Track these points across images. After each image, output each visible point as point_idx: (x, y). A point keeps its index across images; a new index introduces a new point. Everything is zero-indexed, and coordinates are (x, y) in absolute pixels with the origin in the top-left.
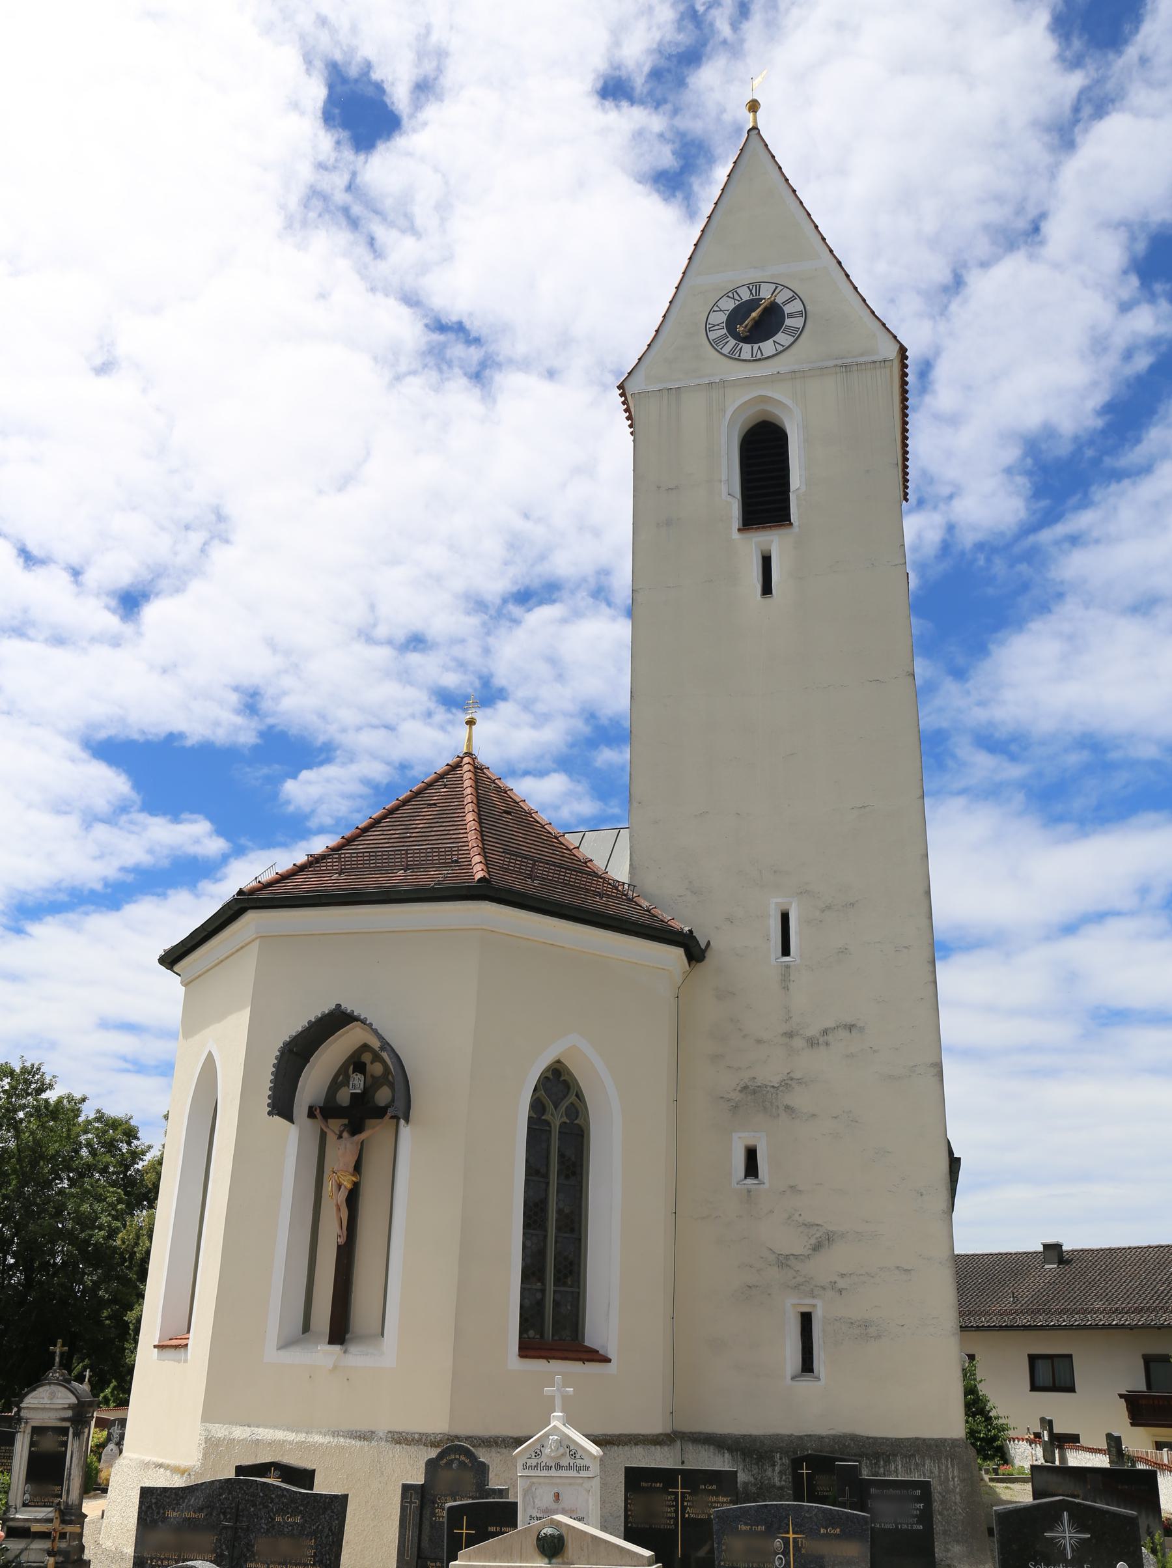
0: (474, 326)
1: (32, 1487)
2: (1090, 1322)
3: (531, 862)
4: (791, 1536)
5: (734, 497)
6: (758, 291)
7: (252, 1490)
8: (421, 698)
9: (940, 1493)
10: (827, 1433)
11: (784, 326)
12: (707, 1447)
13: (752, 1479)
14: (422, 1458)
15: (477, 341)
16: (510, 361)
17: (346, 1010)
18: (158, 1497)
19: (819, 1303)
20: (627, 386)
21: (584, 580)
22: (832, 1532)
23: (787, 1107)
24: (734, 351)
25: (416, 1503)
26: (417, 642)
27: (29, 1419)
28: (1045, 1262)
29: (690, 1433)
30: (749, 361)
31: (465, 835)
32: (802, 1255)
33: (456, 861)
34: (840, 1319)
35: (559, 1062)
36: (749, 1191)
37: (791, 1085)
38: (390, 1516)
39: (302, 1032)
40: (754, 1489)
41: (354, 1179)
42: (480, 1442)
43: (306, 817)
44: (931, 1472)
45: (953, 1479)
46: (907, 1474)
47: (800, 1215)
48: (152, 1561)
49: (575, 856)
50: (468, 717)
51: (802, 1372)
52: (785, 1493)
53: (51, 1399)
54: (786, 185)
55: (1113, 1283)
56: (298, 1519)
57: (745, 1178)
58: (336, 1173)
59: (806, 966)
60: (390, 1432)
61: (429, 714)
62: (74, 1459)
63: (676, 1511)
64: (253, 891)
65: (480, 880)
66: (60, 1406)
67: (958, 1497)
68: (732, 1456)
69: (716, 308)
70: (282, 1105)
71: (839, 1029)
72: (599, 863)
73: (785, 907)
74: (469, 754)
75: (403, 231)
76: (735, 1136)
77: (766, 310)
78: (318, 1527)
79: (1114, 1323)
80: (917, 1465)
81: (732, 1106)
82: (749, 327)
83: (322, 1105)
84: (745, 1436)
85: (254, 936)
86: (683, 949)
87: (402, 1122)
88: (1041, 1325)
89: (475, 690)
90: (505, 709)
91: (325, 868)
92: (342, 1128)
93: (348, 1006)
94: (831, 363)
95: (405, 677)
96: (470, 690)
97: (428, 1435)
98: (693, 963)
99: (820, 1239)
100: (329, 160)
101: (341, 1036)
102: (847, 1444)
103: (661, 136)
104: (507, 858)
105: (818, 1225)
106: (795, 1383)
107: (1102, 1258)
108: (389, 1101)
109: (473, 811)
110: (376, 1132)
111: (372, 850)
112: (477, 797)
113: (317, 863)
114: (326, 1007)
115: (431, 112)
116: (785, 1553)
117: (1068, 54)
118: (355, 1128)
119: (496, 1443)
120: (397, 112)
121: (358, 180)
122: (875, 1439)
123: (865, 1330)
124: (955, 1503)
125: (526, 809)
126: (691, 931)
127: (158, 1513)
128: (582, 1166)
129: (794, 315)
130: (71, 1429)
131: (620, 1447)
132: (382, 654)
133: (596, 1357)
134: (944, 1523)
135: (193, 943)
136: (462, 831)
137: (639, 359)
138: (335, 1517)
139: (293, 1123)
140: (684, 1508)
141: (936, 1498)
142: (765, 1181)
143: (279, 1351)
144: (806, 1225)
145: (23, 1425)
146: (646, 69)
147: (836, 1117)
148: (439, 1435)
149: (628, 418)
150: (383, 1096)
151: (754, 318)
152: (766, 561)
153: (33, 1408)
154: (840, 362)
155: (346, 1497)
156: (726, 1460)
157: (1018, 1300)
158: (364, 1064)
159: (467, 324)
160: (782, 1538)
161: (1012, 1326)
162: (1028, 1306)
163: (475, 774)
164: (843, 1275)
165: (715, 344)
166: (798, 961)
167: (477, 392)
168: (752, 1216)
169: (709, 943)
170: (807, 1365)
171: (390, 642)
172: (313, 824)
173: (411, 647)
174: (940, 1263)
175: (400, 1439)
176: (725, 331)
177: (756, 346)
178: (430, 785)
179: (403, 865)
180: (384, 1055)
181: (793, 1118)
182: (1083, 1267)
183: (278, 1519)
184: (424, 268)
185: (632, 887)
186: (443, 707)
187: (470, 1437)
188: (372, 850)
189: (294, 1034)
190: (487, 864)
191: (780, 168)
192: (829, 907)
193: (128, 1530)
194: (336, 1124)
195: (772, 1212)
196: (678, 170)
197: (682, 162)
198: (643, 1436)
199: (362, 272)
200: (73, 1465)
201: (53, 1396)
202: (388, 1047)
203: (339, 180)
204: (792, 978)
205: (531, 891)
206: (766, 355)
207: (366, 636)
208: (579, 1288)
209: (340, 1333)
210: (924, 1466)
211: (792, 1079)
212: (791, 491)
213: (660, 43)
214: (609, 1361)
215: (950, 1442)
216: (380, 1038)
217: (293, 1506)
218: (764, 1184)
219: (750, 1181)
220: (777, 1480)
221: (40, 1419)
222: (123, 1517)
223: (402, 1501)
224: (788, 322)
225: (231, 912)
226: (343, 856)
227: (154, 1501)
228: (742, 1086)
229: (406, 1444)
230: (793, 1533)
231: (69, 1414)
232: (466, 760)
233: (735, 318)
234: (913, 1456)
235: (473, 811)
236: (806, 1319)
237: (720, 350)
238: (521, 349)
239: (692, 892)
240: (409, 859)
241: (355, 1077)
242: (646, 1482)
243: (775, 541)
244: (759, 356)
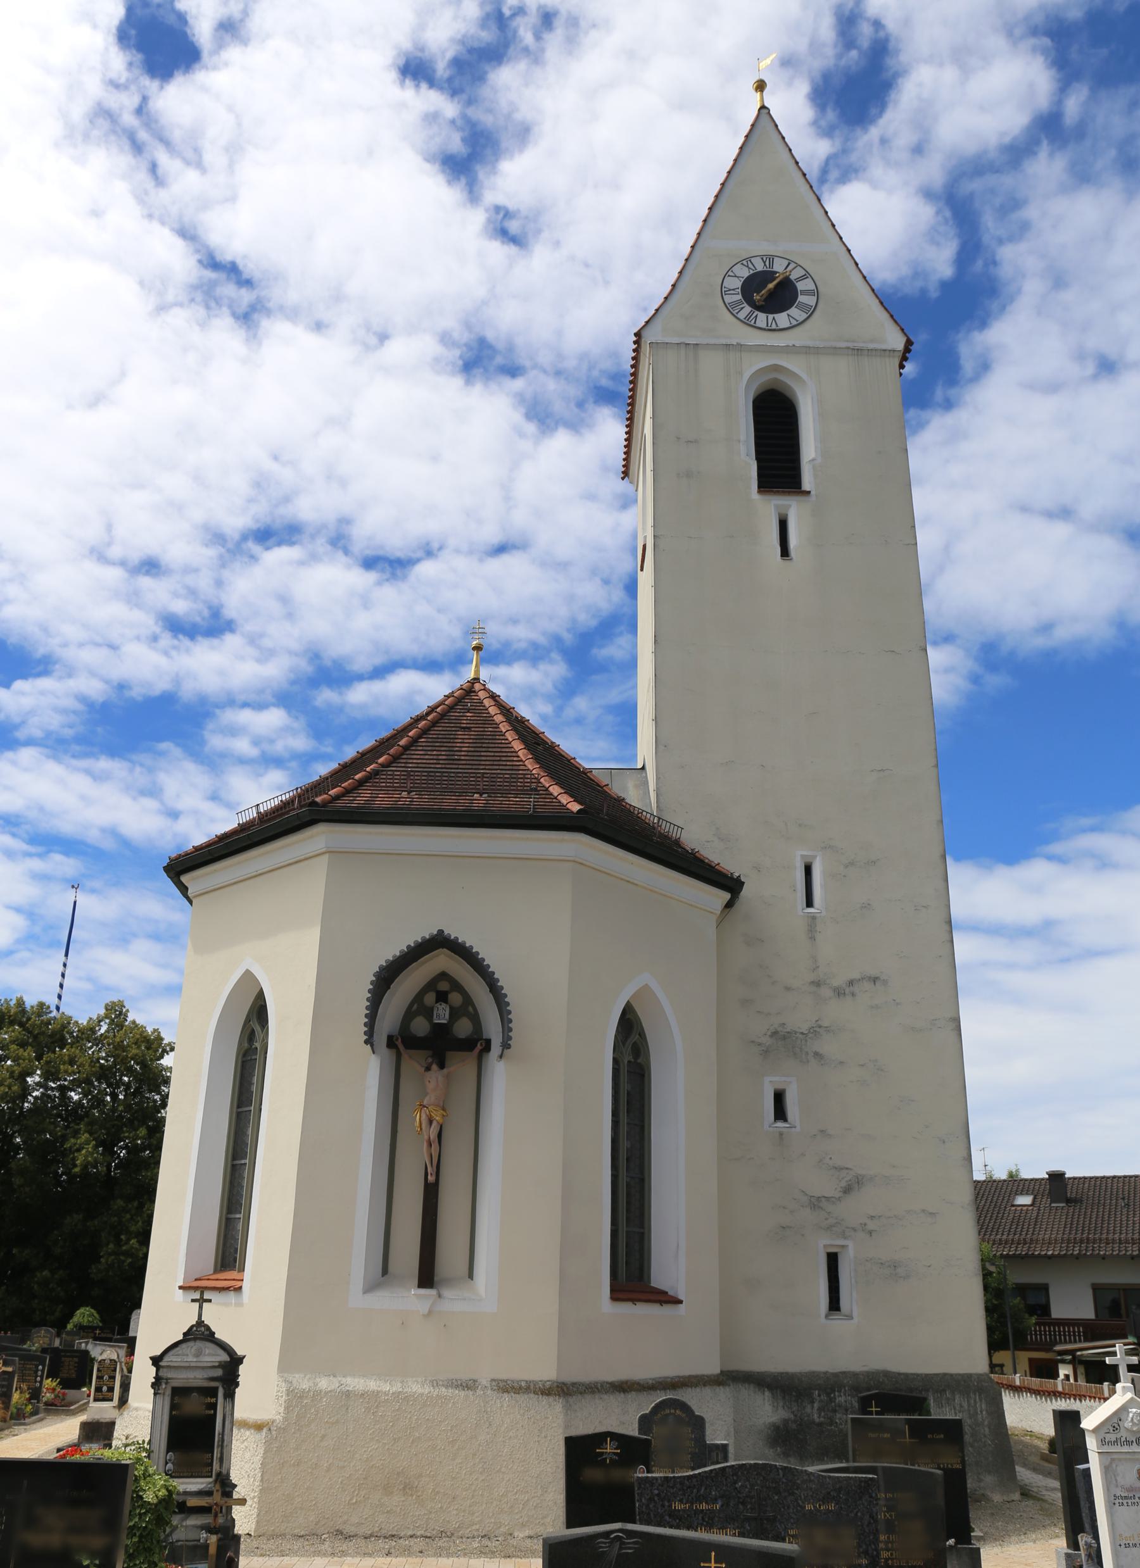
0: (249, 268)
1: (175, 1456)
8: (148, 622)
9: (970, 1426)
10: (861, 1370)
11: (797, 302)
12: (747, 1385)
13: (792, 1416)
14: (534, 1407)
15: (248, 283)
16: (281, 308)
17: (450, 936)
19: (850, 1244)
20: (644, 334)
21: (324, 526)
23: (816, 1054)
24: (750, 317)
26: (151, 566)
27: (170, 1379)
29: (728, 1371)
30: (764, 329)
32: (832, 1197)
33: (535, 790)
34: (871, 1259)
36: (781, 1134)
37: (819, 1032)
38: (501, 1468)
39: (400, 957)
40: (794, 1426)
43: (16, 727)
44: (961, 1406)
45: (981, 1412)
46: (939, 1408)
47: (831, 1158)
52: (824, 1429)
54: (796, 168)
58: (427, 1108)
59: (832, 918)
61: (155, 638)
62: (227, 1423)
67: (987, 1429)
68: (772, 1394)
71: (864, 981)
75: (187, 163)
76: (767, 1080)
78: (856, 1514)
80: (948, 1399)
81: (763, 1050)
82: (764, 297)
84: (782, 1373)
85: (324, 850)
89: (203, 619)
90: (232, 641)
94: (843, 345)
95: (134, 599)
96: (198, 619)
97: (535, 1383)
99: (850, 1183)
100: (120, 78)
101: (426, 962)
102: (881, 1380)
103: (453, 122)
105: (847, 1169)
106: (829, 1322)
111: (466, 771)
115: (233, 53)
117: (823, 123)
120: (197, 44)
121: (151, 104)
122: (906, 1375)
123: (894, 1270)
124: (985, 1436)
127: (663, 1506)
129: (806, 293)
131: (693, 1388)
132: (114, 575)
134: (975, 1454)
137: (656, 310)
141: (967, 1431)
144: (836, 1168)
145: (164, 1386)
146: (450, 55)
147: (862, 1065)
148: (548, 1383)
150: (463, 1028)
151: (770, 290)
152: (783, 525)
153: (174, 1367)
154: (851, 345)
156: (766, 1398)
159: (240, 264)
164: (872, 1217)
166: (824, 913)
167: (242, 333)
168: (784, 1158)
170: (834, 1304)
171: (123, 563)
172: (20, 735)
173: (144, 570)
174: (962, 1207)
176: (740, 297)
177: (771, 316)
178: (451, 708)
181: (822, 1065)
184: (205, 204)
186: (170, 633)
188: (466, 771)
191: (790, 150)
192: (852, 864)
195: (803, 1155)
196: (465, 156)
197: (469, 150)
198: (707, 1376)
199: (141, 198)
201: (198, 1354)
203: (126, 102)
204: (818, 929)
206: (781, 326)
207: (99, 555)
210: (954, 1400)
213: (464, 36)
214: (681, 1302)
215: (976, 1377)
219: (780, 1124)
220: (816, 1416)
221: (183, 1379)
226: (412, 773)
228: (773, 1031)
229: (515, 1393)
231: (219, 1373)
233: (751, 286)
234: (944, 1390)
236: (833, 1260)
237: (736, 315)
238: (292, 297)
239: (719, 838)
241: (439, 1006)
243: (796, 510)
244: (774, 326)
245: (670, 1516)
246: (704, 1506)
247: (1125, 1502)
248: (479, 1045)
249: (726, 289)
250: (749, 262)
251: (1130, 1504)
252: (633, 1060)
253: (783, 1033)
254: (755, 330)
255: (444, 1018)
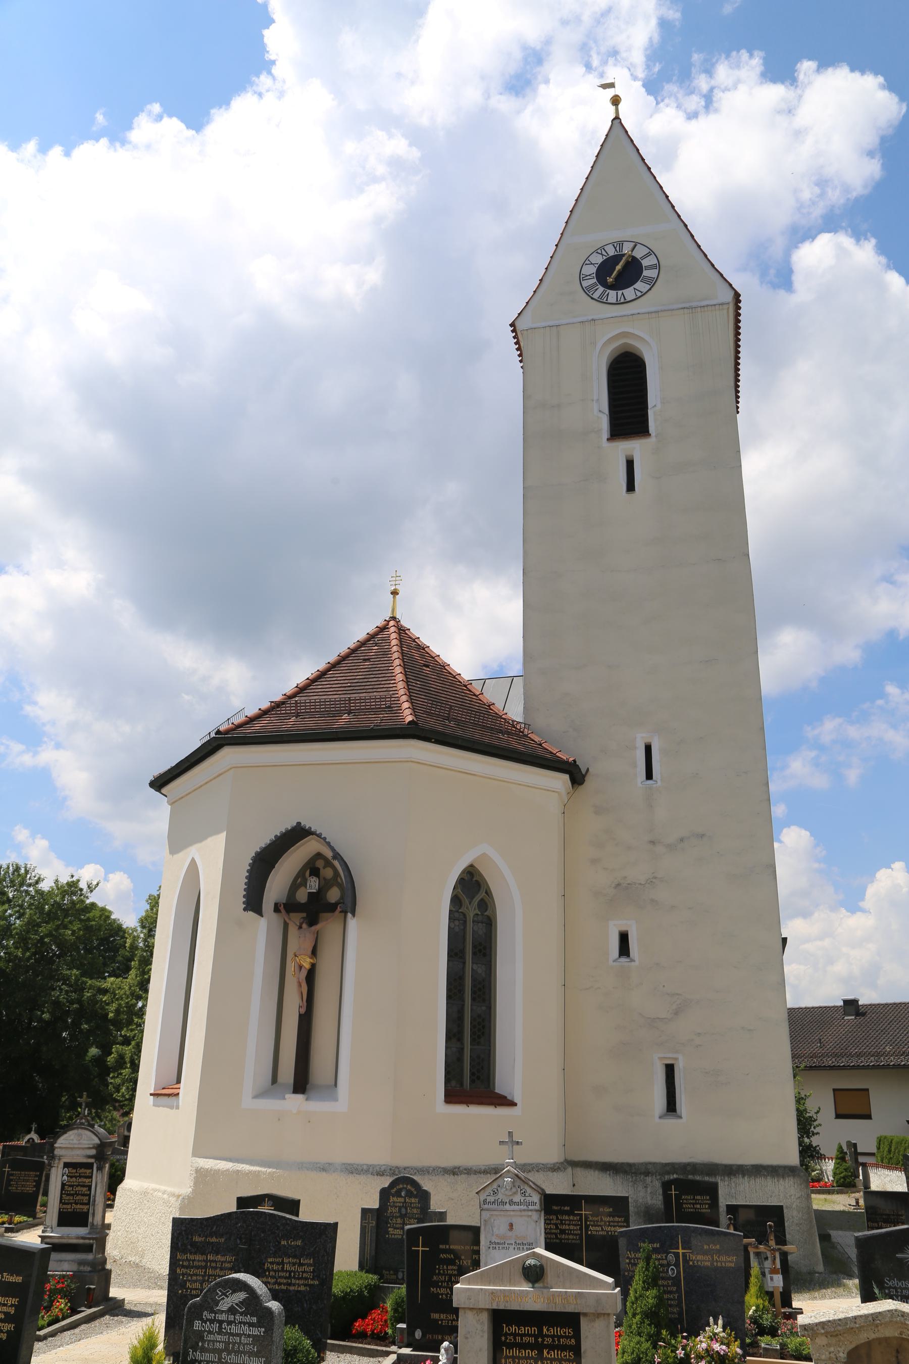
2: (883, 1063)
3: (448, 707)
4: (681, 1251)
5: (602, 412)
6: (621, 249)
7: (262, 1219)
17: (305, 827)
18: (187, 1226)
19: (680, 1057)
20: (517, 324)
22: (714, 1248)
23: (652, 900)
25: (372, 1223)
27: (62, 1156)
28: (846, 1014)
30: (650, 289)
31: (394, 685)
33: (389, 707)
35: (471, 866)
39: (270, 845)
41: (312, 961)
42: (415, 1171)
48: (183, 1277)
49: (480, 700)
50: (393, 589)
51: (667, 1111)
53: (79, 1140)
55: (900, 1031)
56: (299, 1243)
57: (619, 957)
60: (344, 1164)
62: (98, 1188)
63: (581, 1229)
64: (227, 732)
65: (410, 723)
66: (87, 1146)
68: (613, 1180)
69: (587, 262)
70: (254, 903)
72: (499, 706)
73: (648, 741)
74: (393, 618)
76: (611, 924)
77: (627, 264)
78: (315, 1249)
79: (903, 1063)
83: (284, 902)
86: (568, 775)
87: (349, 915)
88: (844, 1066)
91: (284, 712)
92: (302, 920)
93: (307, 823)
97: (374, 1166)
98: (576, 785)
104: (430, 703)
106: (662, 1121)
107: (891, 1010)
108: (338, 899)
109: (400, 665)
110: (329, 926)
112: (402, 653)
113: (278, 707)
114: (289, 824)
116: (677, 1265)
118: (312, 921)
119: (428, 1172)
125: (441, 662)
126: (574, 761)
127: (187, 1238)
128: (491, 948)
130: (95, 1164)
133: (505, 1102)
135: (178, 771)
136: (392, 682)
138: (329, 1241)
139: (262, 916)
140: (587, 1227)
142: (635, 959)
143: (254, 1100)
144: (668, 994)
148: (383, 1167)
149: (518, 349)
150: (333, 895)
152: (630, 464)
155: (336, 1224)
157: (824, 1045)
158: (318, 869)
160: (674, 1253)
161: (820, 1066)
162: (832, 1050)
163: (399, 634)
165: (587, 291)
169: (588, 770)
170: (671, 1106)
175: (353, 1170)
176: (595, 280)
177: (620, 292)
179: (347, 710)
180: (336, 863)
182: (875, 1018)
183: (284, 1243)
185: (527, 726)
187: (408, 1168)
189: (264, 846)
190: (414, 708)
193: (132, 1242)
194: (297, 917)
198: (543, 1164)
200: (97, 1192)
202: (338, 856)
205: (448, 731)
206: (628, 299)
208: (490, 1046)
209: (301, 1084)
211: (655, 878)
212: (649, 407)
214: (515, 1104)
216: (333, 849)
217: (295, 1232)
218: (634, 961)
219: (624, 960)
222: (127, 1232)
223: (361, 1222)
224: (646, 273)
225: (210, 748)
227: (183, 1228)
230: (683, 1249)
231: (93, 1152)
232: (392, 623)
233: (603, 272)
235: (400, 665)
236: (670, 1070)
240: (352, 705)
242: (557, 1206)
243: (634, 447)
244: (622, 300)
245: (191, 1245)
246: (214, 1240)
247: (497, 1246)
248: (339, 907)
249: (584, 276)
250: (603, 250)
251: (501, 1248)
252: (486, 914)
253: (625, 885)
254: (646, 295)
255: (314, 889)
